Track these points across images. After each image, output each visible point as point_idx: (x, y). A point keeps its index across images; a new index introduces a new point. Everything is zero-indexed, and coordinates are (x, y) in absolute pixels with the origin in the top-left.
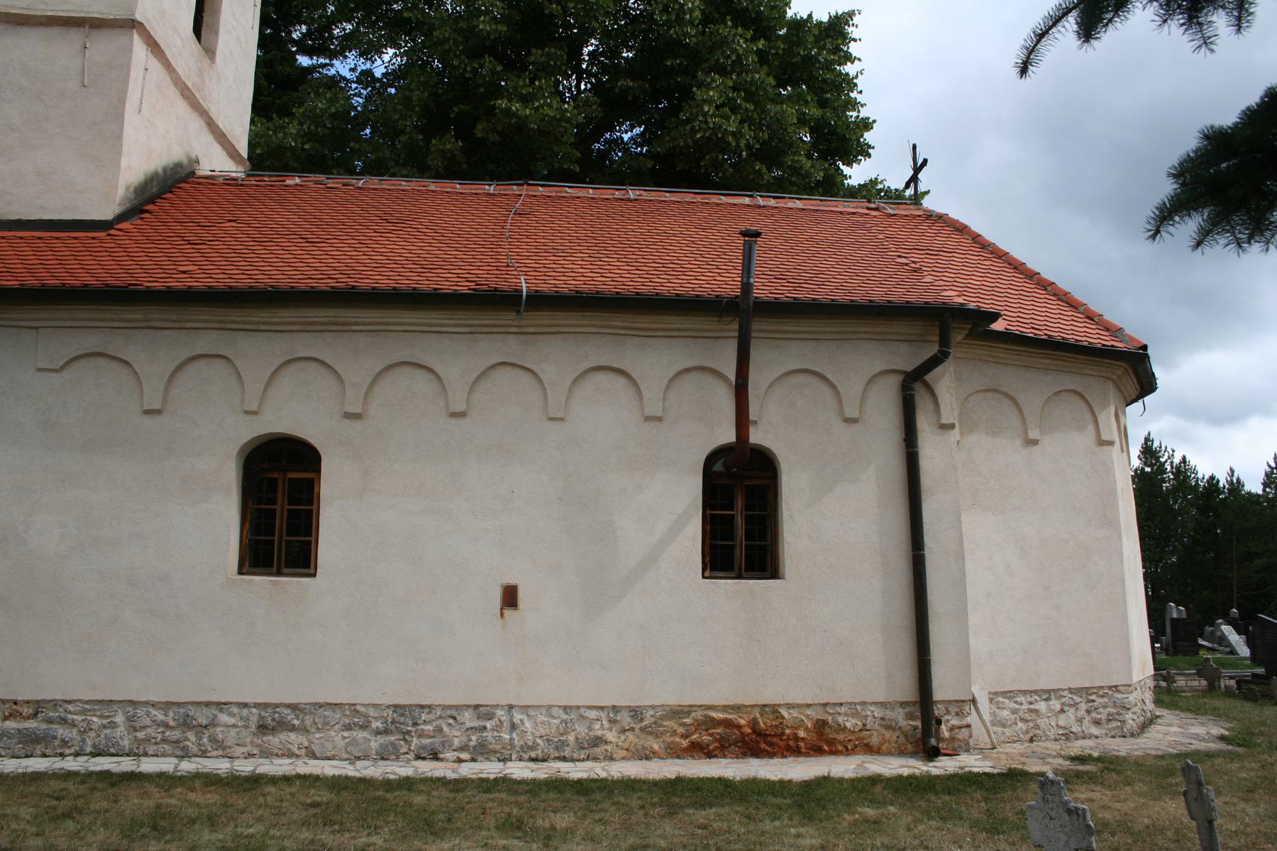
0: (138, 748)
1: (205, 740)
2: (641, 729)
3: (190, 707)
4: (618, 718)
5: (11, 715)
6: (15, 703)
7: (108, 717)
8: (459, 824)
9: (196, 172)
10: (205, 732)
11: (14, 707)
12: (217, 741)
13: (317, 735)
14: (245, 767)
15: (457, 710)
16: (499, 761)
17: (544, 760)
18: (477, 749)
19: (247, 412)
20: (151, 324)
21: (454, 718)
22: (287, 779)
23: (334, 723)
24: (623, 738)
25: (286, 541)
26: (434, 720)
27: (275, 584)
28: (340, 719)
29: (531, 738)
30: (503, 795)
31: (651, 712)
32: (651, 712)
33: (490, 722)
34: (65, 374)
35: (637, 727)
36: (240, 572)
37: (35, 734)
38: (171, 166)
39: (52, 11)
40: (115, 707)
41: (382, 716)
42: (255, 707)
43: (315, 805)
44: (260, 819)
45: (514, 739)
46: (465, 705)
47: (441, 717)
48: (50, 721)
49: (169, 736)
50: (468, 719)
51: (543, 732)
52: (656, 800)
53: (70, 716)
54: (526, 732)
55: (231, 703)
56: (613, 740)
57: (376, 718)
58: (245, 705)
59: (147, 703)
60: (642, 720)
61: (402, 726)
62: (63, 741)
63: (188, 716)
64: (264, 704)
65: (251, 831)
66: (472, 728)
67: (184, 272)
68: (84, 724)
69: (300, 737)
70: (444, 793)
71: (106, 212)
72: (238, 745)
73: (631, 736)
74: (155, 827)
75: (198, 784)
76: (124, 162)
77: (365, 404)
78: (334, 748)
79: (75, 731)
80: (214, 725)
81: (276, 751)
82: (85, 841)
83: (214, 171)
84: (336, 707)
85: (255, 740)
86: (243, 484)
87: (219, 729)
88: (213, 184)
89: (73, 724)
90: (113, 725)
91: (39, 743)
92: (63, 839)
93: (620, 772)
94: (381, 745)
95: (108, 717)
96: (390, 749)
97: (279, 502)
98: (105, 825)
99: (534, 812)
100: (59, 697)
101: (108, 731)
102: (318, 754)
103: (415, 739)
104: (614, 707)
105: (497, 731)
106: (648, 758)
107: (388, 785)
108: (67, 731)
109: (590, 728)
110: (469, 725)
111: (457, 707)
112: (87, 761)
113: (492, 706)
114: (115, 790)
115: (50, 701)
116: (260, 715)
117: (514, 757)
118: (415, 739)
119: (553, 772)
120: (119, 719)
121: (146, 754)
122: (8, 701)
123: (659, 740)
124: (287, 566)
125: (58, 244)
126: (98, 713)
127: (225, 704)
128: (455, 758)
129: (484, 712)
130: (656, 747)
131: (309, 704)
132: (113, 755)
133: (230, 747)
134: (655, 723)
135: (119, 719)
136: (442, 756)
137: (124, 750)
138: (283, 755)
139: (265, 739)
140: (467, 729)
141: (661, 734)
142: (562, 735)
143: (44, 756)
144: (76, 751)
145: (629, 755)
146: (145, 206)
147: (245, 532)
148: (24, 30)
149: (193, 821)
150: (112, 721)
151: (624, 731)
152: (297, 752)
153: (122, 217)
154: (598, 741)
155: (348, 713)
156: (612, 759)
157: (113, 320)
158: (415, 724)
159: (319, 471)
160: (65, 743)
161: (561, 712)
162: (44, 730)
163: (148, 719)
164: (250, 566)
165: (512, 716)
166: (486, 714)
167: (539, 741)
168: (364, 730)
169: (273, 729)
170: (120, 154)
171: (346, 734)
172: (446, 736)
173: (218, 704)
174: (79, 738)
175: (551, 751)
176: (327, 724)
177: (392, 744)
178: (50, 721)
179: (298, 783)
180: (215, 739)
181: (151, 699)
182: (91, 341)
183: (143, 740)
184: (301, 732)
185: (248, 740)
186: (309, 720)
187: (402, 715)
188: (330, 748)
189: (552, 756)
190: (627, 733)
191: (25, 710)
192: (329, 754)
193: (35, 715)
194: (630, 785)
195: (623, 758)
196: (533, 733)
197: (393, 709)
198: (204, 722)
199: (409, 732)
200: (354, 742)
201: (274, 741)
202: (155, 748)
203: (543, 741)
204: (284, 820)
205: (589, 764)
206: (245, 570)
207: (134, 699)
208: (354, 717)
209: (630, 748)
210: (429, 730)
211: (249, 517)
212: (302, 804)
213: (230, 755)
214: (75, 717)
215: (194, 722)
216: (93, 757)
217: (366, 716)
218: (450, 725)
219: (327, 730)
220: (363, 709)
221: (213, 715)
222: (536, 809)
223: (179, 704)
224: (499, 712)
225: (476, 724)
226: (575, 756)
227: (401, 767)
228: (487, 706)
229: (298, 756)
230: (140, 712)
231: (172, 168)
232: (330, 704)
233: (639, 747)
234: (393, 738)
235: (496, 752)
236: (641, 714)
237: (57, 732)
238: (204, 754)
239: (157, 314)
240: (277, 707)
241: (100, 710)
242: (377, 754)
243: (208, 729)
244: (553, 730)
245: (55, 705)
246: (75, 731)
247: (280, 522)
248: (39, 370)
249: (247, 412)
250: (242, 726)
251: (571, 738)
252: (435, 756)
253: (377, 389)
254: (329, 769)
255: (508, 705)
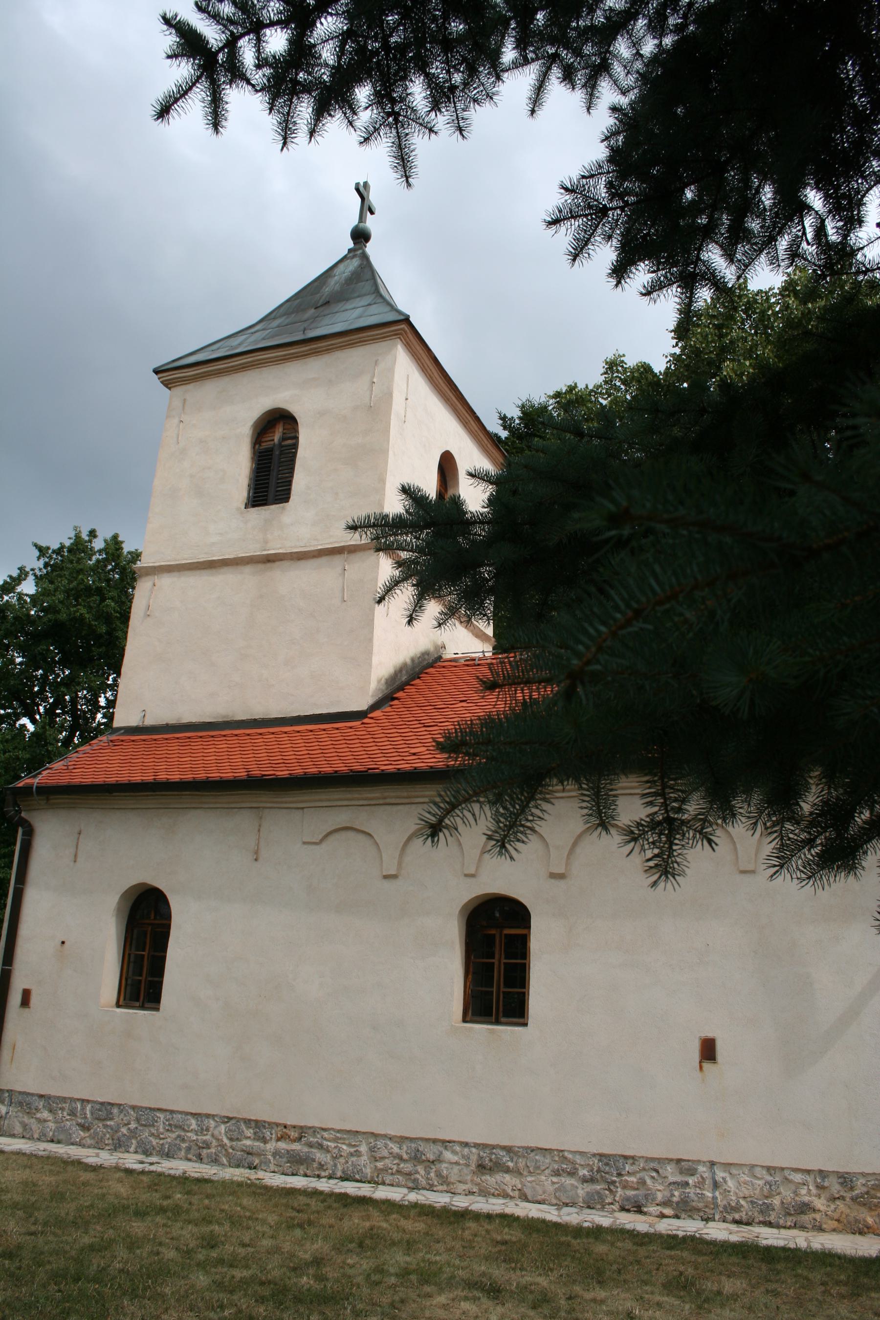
0: (378, 1177)
1: (432, 1175)
2: (852, 1199)
3: (420, 1143)
4: (826, 1184)
5: (282, 1137)
6: (285, 1127)
7: (355, 1146)
8: (628, 1277)
9: (443, 656)
10: (433, 1167)
11: (284, 1130)
12: (443, 1177)
13: (529, 1179)
14: (461, 1203)
15: (659, 1163)
16: (702, 1220)
17: (748, 1224)
18: (680, 1205)
19: (466, 875)
20: (388, 801)
21: (657, 1171)
22: (489, 1217)
23: (543, 1168)
24: (833, 1207)
25: (504, 992)
26: (637, 1172)
27: (492, 1032)
28: (550, 1164)
29: (734, 1198)
30: (685, 1254)
31: (863, 1181)
32: (863, 1181)
33: (693, 1178)
34: (324, 845)
35: (848, 1195)
36: (465, 1020)
37: (299, 1155)
38: (418, 656)
39: (321, 545)
40: (360, 1138)
41: (589, 1164)
42: (474, 1147)
43: (505, 1243)
44: (450, 1250)
45: (717, 1198)
46: (667, 1159)
47: (644, 1169)
48: (310, 1145)
49: (403, 1168)
50: (671, 1173)
51: (747, 1193)
52: (842, 1277)
53: (325, 1143)
54: (729, 1192)
55: (454, 1142)
56: (822, 1208)
57: (582, 1165)
58: (466, 1145)
59: (385, 1136)
60: (852, 1189)
61: (607, 1176)
62: (320, 1164)
63: (418, 1150)
64: (483, 1144)
65: (438, 1258)
66: (674, 1183)
67: (414, 754)
68: (336, 1151)
69: (514, 1179)
70: (628, 1245)
71: (361, 704)
72: (460, 1182)
73: (842, 1206)
74: (361, 1245)
75: (413, 1213)
76: (375, 660)
77: (567, 864)
78: (544, 1192)
79: (329, 1156)
80: (440, 1161)
81: (492, 1191)
82: (304, 1248)
83: (457, 654)
84: (547, 1152)
85: (475, 1179)
86: (466, 940)
87: (444, 1165)
88: (455, 667)
89: (327, 1150)
90: (358, 1154)
91: (302, 1164)
92: (288, 1243)
93: (822, 1244)
94: (588, 1193)
95: (355, 1146)
96: (596, 1198)
97: (497, 956)
98: (325, 1238)
99: (708, 1274)
100: (317, 1124)
101: (354, 1159)
102: (530, 1197)
103: (619, 1189)
104: (821, 1171)
105: (700, 1188)
106: (861, 1233)
107: (578, 1231)
108: (323, 1156)
109: (796, 1193)
110: (672, 1179)
111: (659, 1160)
112: (336, 1184)
113: (693, 1161)
114: (345, 1210)
115: (310, 1128)
116: (479, 1154)
117: (717, 1217)
118: (619, 1189)
119: (750, 1236)
120: (363, 1148)
121: (383, 1183)
122: (280, 1124)
123: (873, 1213)
124: (506, 1015)
125: (323, 735)
126: (347, 1142)
127: (449, 1142)
128: (658, 1213)
129: (686, 1167)
130: (870, 1220)
131: (522, 1147)
132: (357, 1181)
133: (453, 1184)
134: (867, 1193)
135: (363, 1148)
136: (645, 1209)
137: (366, 1178)
138: (499, 1195)
139: (483, 1178)
140: (670, 1184)
141: (876, 1206)
142: (767, 1197)
143: (306, 1175)
144: (330, 1174)
145: (840, 1226)
146: (395, 693)
147: (468, 984)
148: (302, 563)
149: (393, 1243)
150: (357, 1151)
151: (833, 1199)
152: (511, 1194)
153: (374, 707)
154: (805, 1208)
155: (557, 1158)
156: (821, 1229)
157: (359, 799)
158: (619, 1175)
159: (529, 927)
160: (321, 1166)
161: (764, 1172)
162: (306, 1153)
163: (386, 1151)
164: (473, 1015)
165: (714, 1173)
166: (688, 1170)
167: (742, 1202)
168: (572, 1177)
169: (490, 1169)
170: (372, 653)
171: (555, 1179)
172: (649, 1189)
173: (444, 1142)
174: (332, 1163)
175: (756, 1214)
176: (538, 1168)
177: (598, 1193)
178: (310, 1145)
179: (497, 1221)
180: (440, 1174)
181: (389, 1132)
182: (342, 817)
183: (381, 1170)
184: (515, 1174)
185: (469, 1178)
186: (521, 1163)
187: (607, 1164)
188: (540, 1192)
189: (757, 1220)
190: (838, 1202)
191: (293, 1134)
192: (539, 1198)
193: (299, 1139)
194: (826, 1258)
195: (834, 1230)
196: (736, 1194)
197: (598, 1157)
198: (431, 1157)
199: (614, 1182)
200: (562, 1188)
201: (490, 1180)
202: (391, 1178)
203: (747, 1202)
204: (472, 1253)
205: (794, 1232)
206: (468, 1019)
207: (376, 1132)
208: (562, 1163)
209: (842, 1219)
210: (633, 1182)
211: (471, 970)
212: (492, 1240)
213: (452, 1191)
214: (329, 1144)
215: (423, 1157)
216: (342, 1181)
217: (573, 1163)
218: (653, 1177)
219: (538, 1174)
220: (570, 1156)
221: (439, 1151)
222: (712, 1271)
223: (411, 1140)
224: (701, 1169)
225: (679, 1178)
226: (781, 1222)
227: (603, 1216)
228: (689, 1161)
229: (512, 1198)
230: (380, 1144)
231: (420, 657)
232: (541, 1149)
233: (851, 1219)
234: (599, 1187)
235: (699, 1210)
236: (851, 1181)
237: (315, 1156)
238: (431, 1188)
239: (391, 792)
240: (493, 1148)
241: (348, 1139)
242: (584, 1202)
243: (435, 1165)
244: (757, 1192)
245: (314, 1132)
246: (329, 1156)
247: (498, 974)
248: (304, 843)
249: (466, 875)
250: (463, 1164)
251: (776, 1201)
252: (639, 1210)
253: (578, 850)
254: (533, 1211)
255: (710, 1162)
